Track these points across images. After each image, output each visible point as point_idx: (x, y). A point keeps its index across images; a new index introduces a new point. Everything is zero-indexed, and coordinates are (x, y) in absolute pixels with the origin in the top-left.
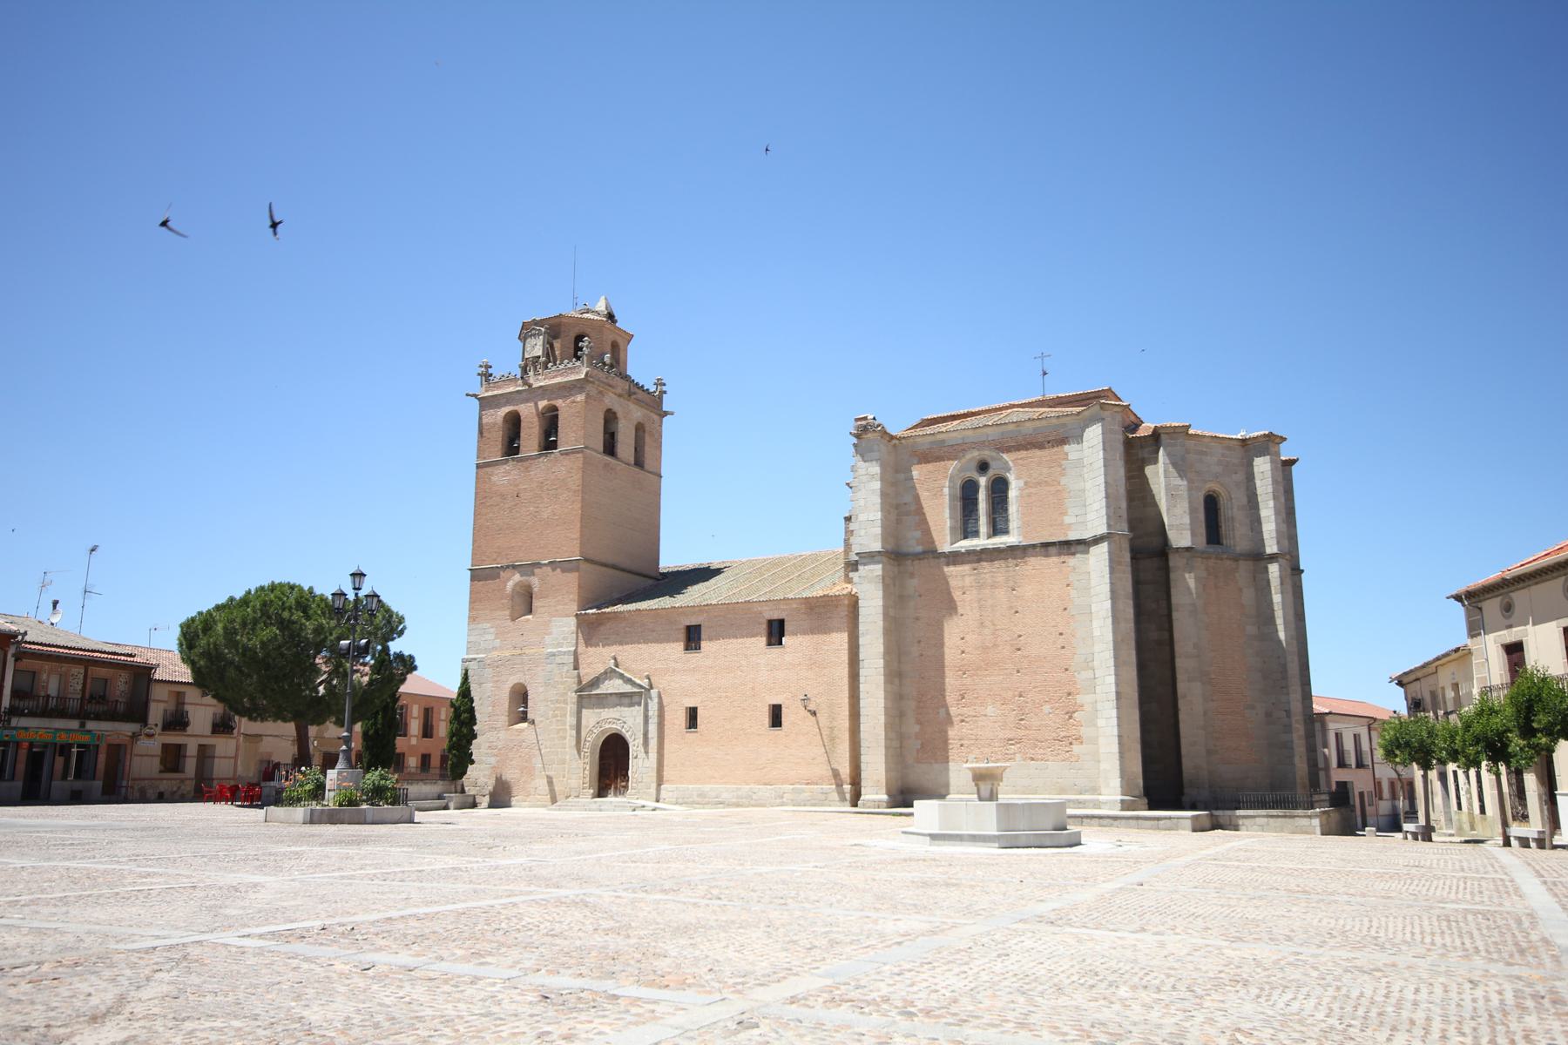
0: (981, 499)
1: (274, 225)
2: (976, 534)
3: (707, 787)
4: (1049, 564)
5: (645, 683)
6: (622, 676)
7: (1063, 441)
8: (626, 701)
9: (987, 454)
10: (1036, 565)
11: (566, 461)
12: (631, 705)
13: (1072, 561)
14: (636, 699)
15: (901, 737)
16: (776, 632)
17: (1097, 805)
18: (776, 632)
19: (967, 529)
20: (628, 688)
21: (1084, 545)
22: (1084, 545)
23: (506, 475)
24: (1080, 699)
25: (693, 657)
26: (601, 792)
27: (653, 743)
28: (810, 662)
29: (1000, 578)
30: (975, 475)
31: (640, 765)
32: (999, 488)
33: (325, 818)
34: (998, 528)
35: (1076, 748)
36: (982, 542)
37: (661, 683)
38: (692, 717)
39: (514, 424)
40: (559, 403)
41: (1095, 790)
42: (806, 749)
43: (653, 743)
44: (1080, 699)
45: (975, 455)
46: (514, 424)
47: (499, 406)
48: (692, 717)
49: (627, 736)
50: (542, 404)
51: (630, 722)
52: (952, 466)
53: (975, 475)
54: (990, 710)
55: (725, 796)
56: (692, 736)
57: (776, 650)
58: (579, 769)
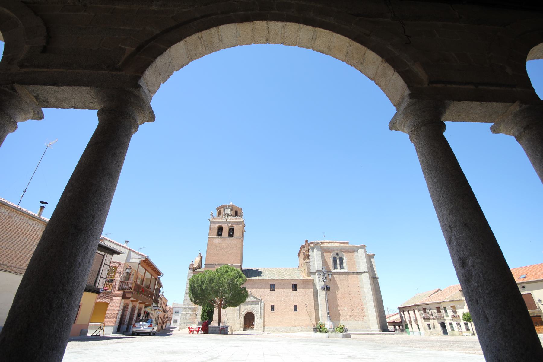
0: (338, 260)
1: (25, 192)
2: (337, 269)
3: (278, 327)
4: (355, 276)
5: (260, 298)
6: (253, 296)
7: (354, 252)
8: (254, 303)
9: (338, 252)
10: (351, 276)
11: (236, 240)
12: (256, 304)
13: (359, 276)
14: (257, 303)
15: (214, 340)
16: (295, 287)
17: (371, 331)
18: (295, 287)
19: (335, 267)
20: (255, 300)
21: (361, 273)
22: (361, 273)
23: (218, 241)
24: (364, 306)
25: (273, 292)
26: (245, 329)
27: (262, 315)
28: (303, 297)
29: (344, 279)
30: (336, 256)
31: (258, 321)
32: (341, 260)
33: (316, 303)
34: (342, 268)
35: (364, 318)
36: (339, 270)
37: (262, 298)
38: (273, 308)
39: (220, 229)
40: (234, 226)
41: (370, 327)
42: (305, 318)
43: (262, 315)
44: (364, 306)
45: (336, 252)
46: (220, 229)
47: (216, 224)
48: (273, 308)
49: (254, 313)
50: (230, 225)
51: (255, 309)
52: (332, 254)
53: (336, 256)
54: (345, 308)
55: (283, 330)
56: (273, 313)
57: (295, 292)
58: (240, 322)
